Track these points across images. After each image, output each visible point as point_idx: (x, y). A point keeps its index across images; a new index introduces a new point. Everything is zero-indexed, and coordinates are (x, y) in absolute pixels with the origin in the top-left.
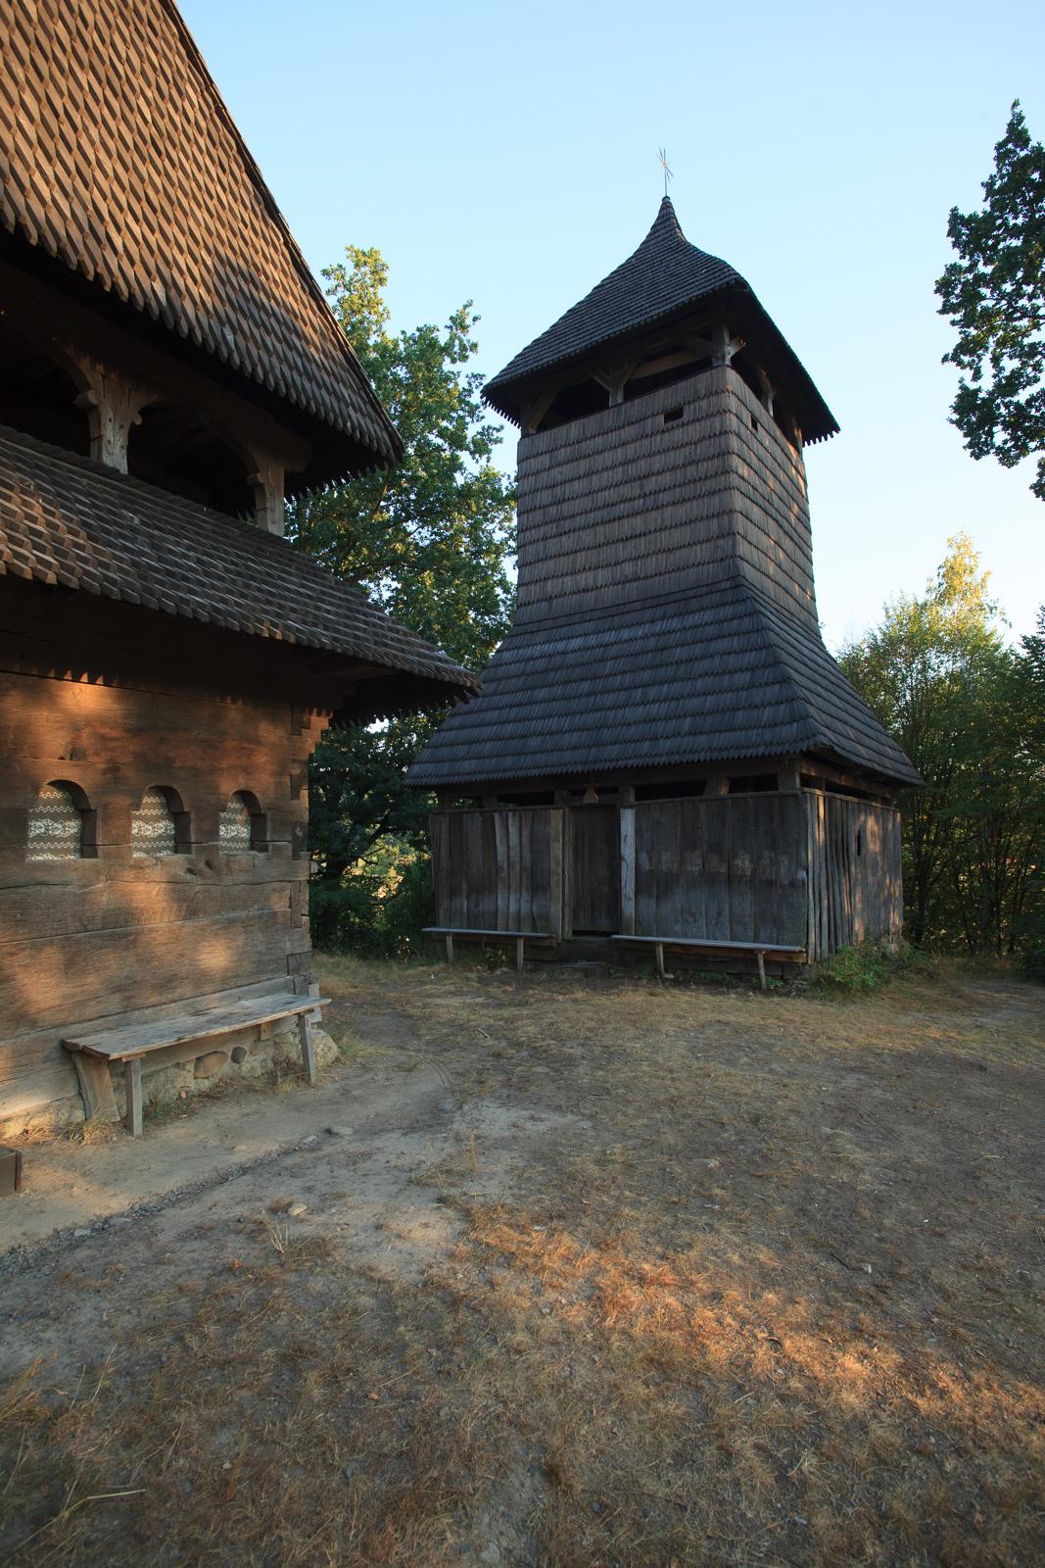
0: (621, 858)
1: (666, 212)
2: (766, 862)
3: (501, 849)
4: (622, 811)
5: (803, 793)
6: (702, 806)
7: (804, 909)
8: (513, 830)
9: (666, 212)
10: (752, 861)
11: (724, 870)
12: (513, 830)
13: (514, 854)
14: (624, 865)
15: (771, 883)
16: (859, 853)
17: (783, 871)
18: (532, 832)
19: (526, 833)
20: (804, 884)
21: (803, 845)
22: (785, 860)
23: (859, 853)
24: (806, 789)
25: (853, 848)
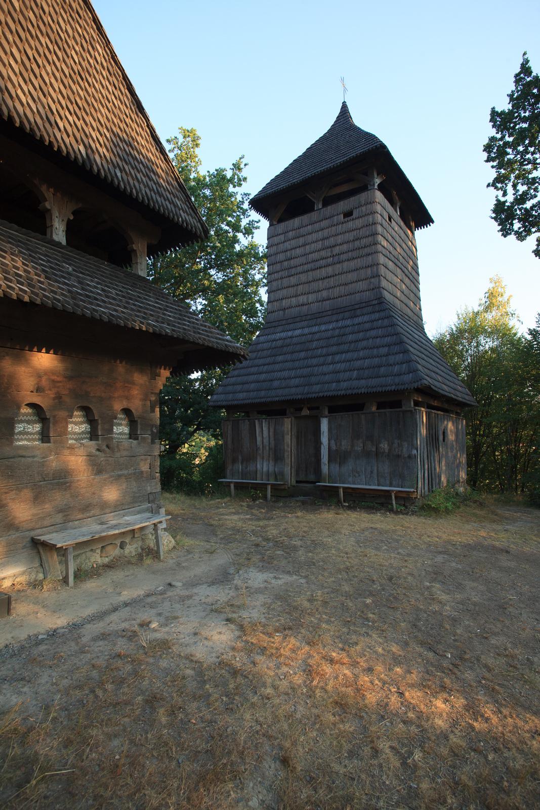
0: (321, 443)
1: (344, 110)
2: (396, 445)
3: (259, 439)
4: (321, 419)
5: (415, 410)
6: (363, 417)
7: (415, 470)
8: (265, 429)
9: (344, 110)
10: (388, 445)
11: (374, 449)
12: (265, 429)
13: (266, 441)
14: (322, 447)
15: (398, 456)
16: (444, 441)
17: (405, 450)
18: (275, 430)
19: (272, 430)
20: (415, 457)
21: (415, 436)
22: (405, 444)
23: (444, 441)
24: (416, 408)
25: (441, 438)
